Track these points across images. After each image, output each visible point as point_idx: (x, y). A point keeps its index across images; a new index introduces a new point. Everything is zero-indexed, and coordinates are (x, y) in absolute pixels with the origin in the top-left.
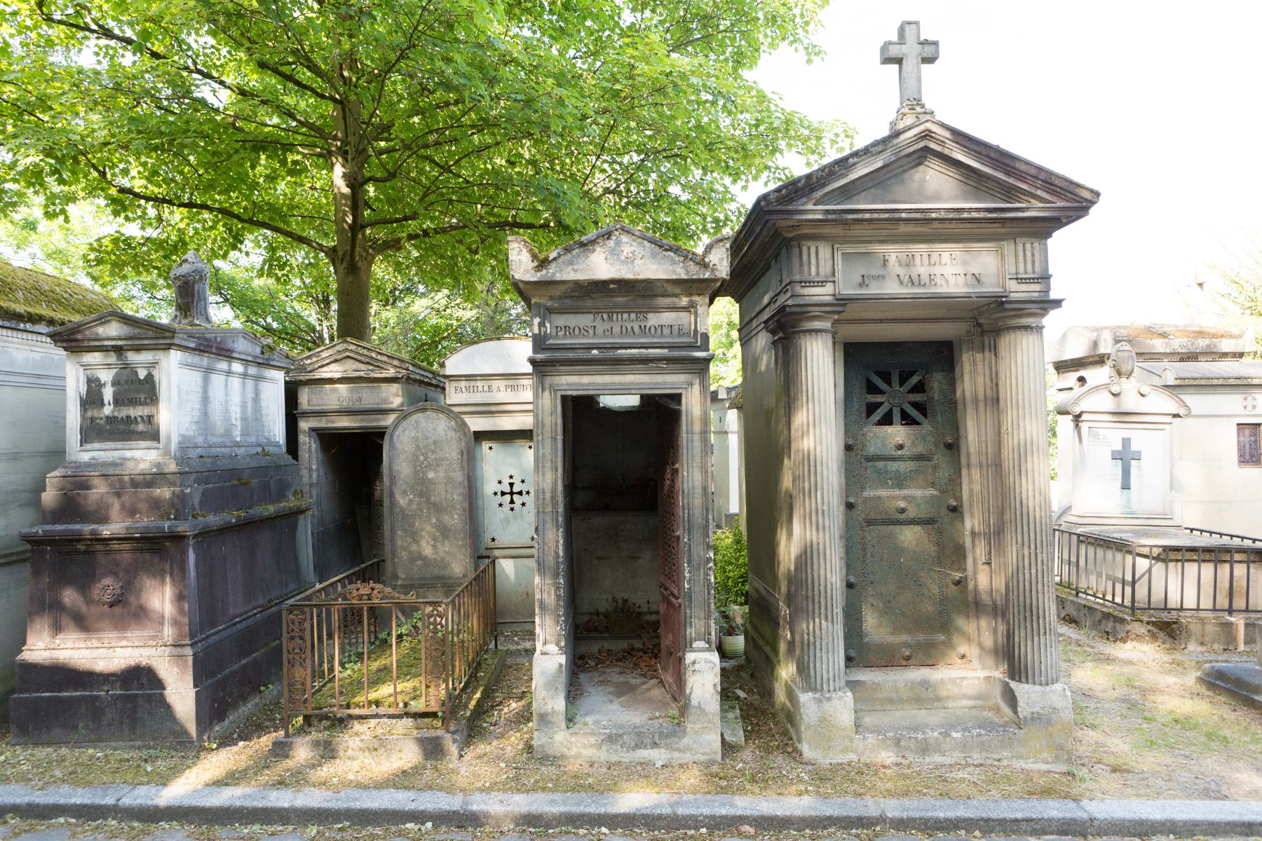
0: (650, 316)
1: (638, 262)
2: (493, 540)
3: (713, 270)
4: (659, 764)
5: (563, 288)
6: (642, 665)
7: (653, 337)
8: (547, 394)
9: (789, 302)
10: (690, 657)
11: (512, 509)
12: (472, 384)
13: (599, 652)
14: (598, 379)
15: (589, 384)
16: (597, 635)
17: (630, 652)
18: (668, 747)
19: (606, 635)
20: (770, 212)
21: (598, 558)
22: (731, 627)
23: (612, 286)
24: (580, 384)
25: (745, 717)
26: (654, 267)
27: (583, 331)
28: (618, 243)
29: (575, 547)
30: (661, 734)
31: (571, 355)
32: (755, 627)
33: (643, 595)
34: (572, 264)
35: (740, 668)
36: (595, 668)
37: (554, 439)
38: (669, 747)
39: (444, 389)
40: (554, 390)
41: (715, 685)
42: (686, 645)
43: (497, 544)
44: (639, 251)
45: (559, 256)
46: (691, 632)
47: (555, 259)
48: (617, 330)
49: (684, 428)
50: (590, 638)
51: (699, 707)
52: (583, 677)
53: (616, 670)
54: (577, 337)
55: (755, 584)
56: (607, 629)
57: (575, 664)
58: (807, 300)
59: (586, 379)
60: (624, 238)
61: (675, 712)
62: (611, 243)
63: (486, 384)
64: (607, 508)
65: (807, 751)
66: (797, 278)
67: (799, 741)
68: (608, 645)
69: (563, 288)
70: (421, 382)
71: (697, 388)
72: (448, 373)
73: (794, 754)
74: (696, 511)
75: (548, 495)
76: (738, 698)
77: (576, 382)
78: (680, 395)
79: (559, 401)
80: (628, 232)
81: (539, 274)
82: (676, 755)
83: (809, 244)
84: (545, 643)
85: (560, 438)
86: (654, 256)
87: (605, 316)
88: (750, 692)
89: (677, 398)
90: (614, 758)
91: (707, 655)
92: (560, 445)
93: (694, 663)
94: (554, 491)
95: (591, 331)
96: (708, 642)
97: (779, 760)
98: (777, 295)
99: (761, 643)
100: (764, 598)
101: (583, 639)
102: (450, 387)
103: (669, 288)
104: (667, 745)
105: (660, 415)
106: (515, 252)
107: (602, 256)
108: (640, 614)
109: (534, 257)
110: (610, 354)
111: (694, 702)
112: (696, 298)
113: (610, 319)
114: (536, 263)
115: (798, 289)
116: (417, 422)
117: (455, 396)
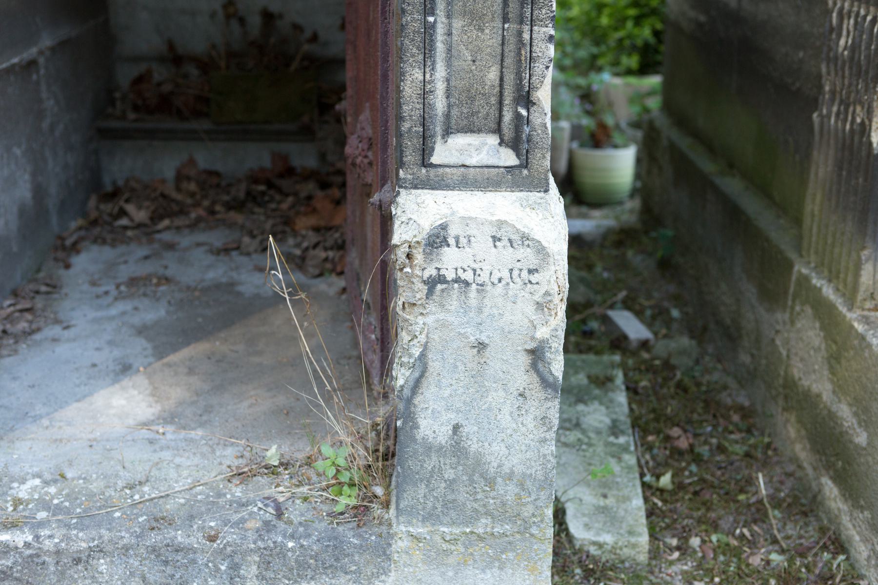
10: (416, 212)
13: (180, 177)
16: (170, 124)
19: (205, 125)
22: (602, 126)
25: (646, 424)
35: (622, 238)
36: (146, 230)
41: (537, 354)
46: (427, 81)
50: (151, 135)
51: (457, 447)
53: (217, 238)
61: (341, 446)
68: (207, 156)
76: (619, 342)
88: (655, 318)
91: (505, 206)
93: (437, 240)
99: (707, 166)
101: (125, 135)
111: (432, 423)
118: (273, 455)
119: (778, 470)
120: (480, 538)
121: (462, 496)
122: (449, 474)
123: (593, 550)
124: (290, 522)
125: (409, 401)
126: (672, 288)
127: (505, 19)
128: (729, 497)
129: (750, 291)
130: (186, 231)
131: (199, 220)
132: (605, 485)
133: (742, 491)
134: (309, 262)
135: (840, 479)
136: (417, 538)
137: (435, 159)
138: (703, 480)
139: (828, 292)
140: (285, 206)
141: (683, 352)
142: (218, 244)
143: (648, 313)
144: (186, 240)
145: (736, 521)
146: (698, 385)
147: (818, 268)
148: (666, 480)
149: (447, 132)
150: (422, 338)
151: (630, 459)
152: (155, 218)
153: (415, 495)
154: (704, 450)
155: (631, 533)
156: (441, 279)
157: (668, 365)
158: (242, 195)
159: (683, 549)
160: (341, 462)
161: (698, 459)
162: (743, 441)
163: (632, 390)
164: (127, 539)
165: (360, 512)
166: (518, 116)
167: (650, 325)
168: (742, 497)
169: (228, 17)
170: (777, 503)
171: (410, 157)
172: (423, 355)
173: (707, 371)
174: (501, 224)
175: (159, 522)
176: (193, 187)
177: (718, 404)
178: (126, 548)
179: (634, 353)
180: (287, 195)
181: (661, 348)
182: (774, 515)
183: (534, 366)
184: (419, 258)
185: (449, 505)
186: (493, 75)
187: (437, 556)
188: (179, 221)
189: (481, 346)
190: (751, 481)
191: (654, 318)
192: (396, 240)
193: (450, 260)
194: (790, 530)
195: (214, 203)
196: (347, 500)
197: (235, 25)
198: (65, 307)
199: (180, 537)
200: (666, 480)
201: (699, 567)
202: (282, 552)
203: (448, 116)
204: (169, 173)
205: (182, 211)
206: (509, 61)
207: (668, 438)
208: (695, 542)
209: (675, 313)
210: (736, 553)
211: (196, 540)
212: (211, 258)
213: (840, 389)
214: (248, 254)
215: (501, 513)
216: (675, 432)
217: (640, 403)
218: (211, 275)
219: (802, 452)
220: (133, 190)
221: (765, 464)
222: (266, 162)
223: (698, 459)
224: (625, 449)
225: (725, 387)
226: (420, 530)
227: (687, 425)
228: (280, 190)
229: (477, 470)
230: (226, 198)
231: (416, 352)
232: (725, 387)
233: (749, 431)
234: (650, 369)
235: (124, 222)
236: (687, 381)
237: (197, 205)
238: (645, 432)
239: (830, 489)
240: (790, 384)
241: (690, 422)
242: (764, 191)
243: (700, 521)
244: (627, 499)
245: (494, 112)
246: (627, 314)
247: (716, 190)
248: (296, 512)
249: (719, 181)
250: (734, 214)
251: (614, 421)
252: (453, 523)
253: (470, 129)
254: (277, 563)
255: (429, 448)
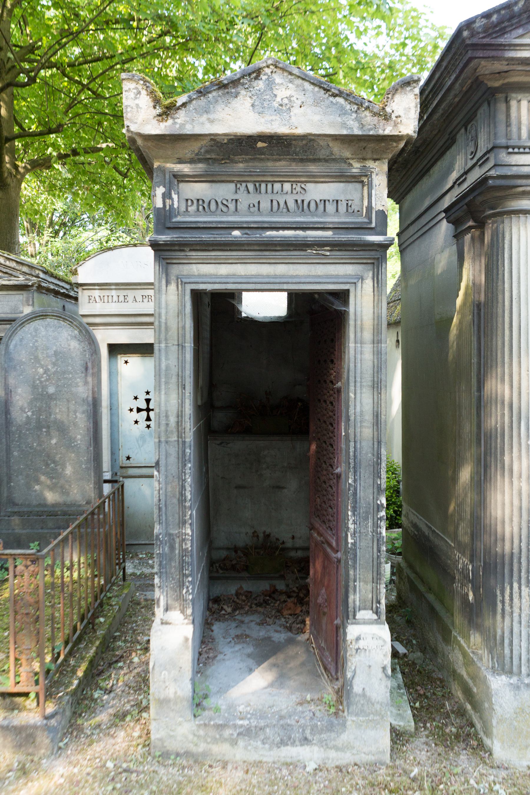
0: (310, 186)
1: (296, 110)
2: (128, 458)
3: (396, 125)
4: (311, 767)
5: (196, 146)
6: (285, 612)
7: (313, 215)
8: (173, 287)
9: (492, 173)
10: (352, 631)
11: (148, 427)
12: (106, 293)
13: (237, 594)
14: (241, 270)
15: (227, 276)
17: (273, 593)
18: (323, 744)
19: (245, 574)
20: (475, 47)
21: (238, 487)
23: (260, 145)
24: (216, 276)
26: (317, 118)
27: (221, 205)
28: (270, 84)
29: (210, 474)
30: (314, 728)
31: (205, 237)
32: (410, 566)
33: (289, 527)
34: (207, 112)
36: (231, 615)
37: (181, 346)
38: (324, 744)
39: (76, 299)
40: (181, 281)
41: (384, 669)
42: (347, 615)
43: (132, 462)
44: (298, 97)
45: (191, 100)
47: (184, 105)
48: (265, 205)
49: (352, 335)
50: (227, 578)
51: (364, 695)
52: (218, 628)
53: (256, 618)
54: (213, 213)
55: (412, 517)
56: (246, 568)
57: (209, 609)
58: (514, 170)
59: (224, 270)
60: (278, 78)
61: (329, 696)
62: (260, 85)
63: (122, 293)
64: (247, 431)
65: (499, 750)
66: (502, 141)
67: (488, 733)
68: (247, 586)
69: (196, 146)
70: (56, 293)
71: (368, 284)
72: (80, 282)
73: (480, 750)
74: (364, 444)
75: (173, 420)
77: (213, 273)
78: (346, 293)
79: (188, 298)
80: (283, 69)
81: (163, 125)
82: (332, 754)
83: (520, 96)
84: (167, 610)
85: (189, 345)
86: (317, 103)
87: (251, 186)
89: (343, 296)
90: (254, 757)
92: (189, 356)
93: (358, 639)
94: (180, 415)
95: (232, 206)
96: (377, 613)
97: (464, 760)
98: (466, 173)
99: (422, 588)
100: (427, 538)
101: (218, 578)
102: (83, 295)
103: (337, 149)
104: (321, 741)
105: (318, 319)
106: (132, 95)
107: (248, 102)
108: (283, 549)
109: (157, 102)
110: (257, 236)
111: (357, 688)
112: (370, 164)
113: (257, 190)
114: (159, 110)
115: (503, 157)
116: (36, 330)
117: (88, 305)
118: (308, 697)
119: (453, 701)
120: (370, 721)
121: (365, 708)
122: (362, 702)
123: (398, 728)
124: (317, 717)
125: (351, 682)
126: (412, 631)
127: (373, 582)
128: (438, 710)
129: (440, 638)
130: (245, 615)
131: (248, 611)
132: (398, 706)
133: (442, 708)
134: (293, 629)
135: (471, 703)
136: (353, 721)
137: (357, 617)
138: (429, 705)
139: (462, 642)
140: (276, 605)
141: (418, 658)
142: (258, 621)
143: (405, 642)
144: (247, 619)
145: (441, 718)
146: (425, 670)
147: (459, 634)
148: (417, 705)
149: (359, 610)
150: (355, 664)
151: (405, 698)
152: (234, 610)
153: (353, 708)
154: (429, 694)
155: (408, 722)
156: (359, 649)
157: (414, 663)
158: (262, 601)
159: (425, 727)
160: (330, 699)
161: (427, 697)
162: (441, 691)
163: (403, 673)
164: (274, 722)
165: (336, 714)
166: (377, 607)
167: (406, 647)
168: (442, 710)
169: (253, 536)
170: (453, 712)
171: (351, 617)
172: (355, 669)
173: (427, 665)
174: (374, 634)
175: (281, 717)
176: (244, 598)
177: (432, 677)
178: (274, 726)
179: (402, 659)
180: (277, 601)
181: (411, 656)
182: (453, 716)
183: (383, 671)
184: (354, 643)
185: (362, 711)
186: (370, 596)
187: (359, 726)
188: (242, 611)
189: (370, 666)
190: (444, 705)
191: (407, 644)
192: (348, 638)
193: (361, 644)
194: (458, 721)
195: (252, 604)
196: (333, 710)
197: (255, 538)
198: (220, 648)
199: (289, 722)
200: (417, 705)
201: (430, 732)
202: (317, 726)
203: (359, 606)
204: (233, 592)
205: (242, 608)
206: (374, 593)
207: (416, 690)
208: (428, 725)
209: (414, 642)
210: (442, 728)
211: (293, 722)
212: (258, 627)
213: (468, 674)
214: (270, 625)
215: (376, 713)
216: (419, 688)
217: (406, 678)
218: (261, 634)
219: (459, 694)
220: (224, 600)
221: (448, 699)
222: (267, 587)
223: (427, 697)
224: (403, 694)
225: (434, 671)
226: (354, 718)
227: (422, 685)
228: (274, 599)
229: (369, 700)
230: (256, 602)
231: (353, 668)
232: (434, 671)
233: (443, 687)
234: (408, 665)
235: (223, 612)
236: (421, 670)
237: (246, 605)
238: (409, 688)
239: (469, 707)
240: (454, 671)
241: (423, 684)
242: (442, 602)
243: (429, 718)
244: (406, 711)
245: (371, 605)
246: (397, 643)
247: (425, 598)
248: (318, 714)
249: (426, 595)
250: (432, 609)
251: (399, 685)
252: (363, 716)
253: (365, 609)
254: (315, 729)
255: (356, 695)
